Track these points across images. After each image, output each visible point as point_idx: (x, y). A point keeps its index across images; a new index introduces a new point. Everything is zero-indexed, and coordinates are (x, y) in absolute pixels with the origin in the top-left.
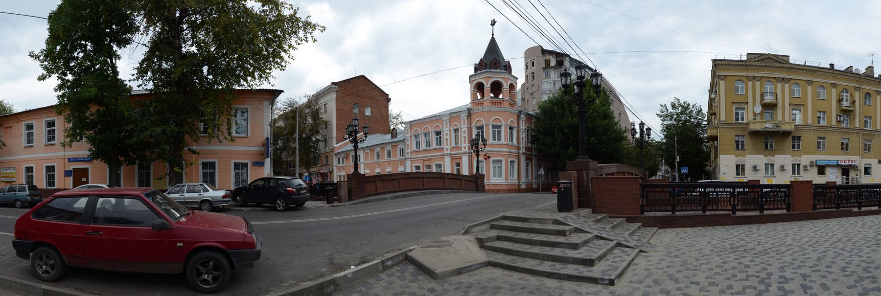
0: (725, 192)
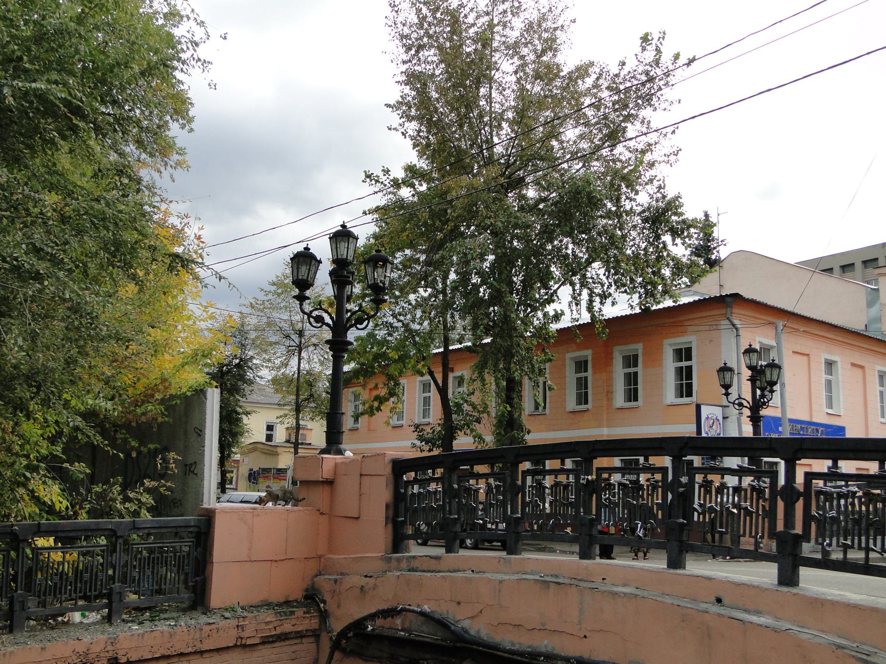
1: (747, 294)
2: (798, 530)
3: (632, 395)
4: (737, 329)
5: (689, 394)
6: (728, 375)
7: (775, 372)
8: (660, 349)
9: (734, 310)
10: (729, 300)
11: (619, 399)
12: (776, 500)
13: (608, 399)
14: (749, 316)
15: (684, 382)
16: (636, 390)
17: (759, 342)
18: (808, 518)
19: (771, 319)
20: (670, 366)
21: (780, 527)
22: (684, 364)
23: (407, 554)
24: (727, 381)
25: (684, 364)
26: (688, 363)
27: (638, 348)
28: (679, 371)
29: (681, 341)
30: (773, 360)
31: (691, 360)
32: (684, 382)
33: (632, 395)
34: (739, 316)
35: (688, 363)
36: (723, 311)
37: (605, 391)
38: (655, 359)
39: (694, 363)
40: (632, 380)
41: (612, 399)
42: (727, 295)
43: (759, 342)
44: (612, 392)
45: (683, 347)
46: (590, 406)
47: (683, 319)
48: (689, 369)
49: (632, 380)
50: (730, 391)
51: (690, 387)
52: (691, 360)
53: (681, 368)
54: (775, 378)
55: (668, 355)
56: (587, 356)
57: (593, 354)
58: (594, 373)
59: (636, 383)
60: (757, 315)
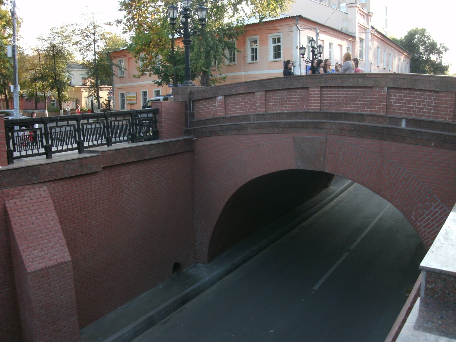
0: (88, 123)
1: (304, 16)
2: (12, 148)
3: (254, 58)
4: (299, 31)
5: (279, 57)
6: (303, 50)
7: (321, 49)
8: (267, 38)
9: (299, 22)
10: (297, 18)
11: (249, 59)
12: (12, 136)
13: (244, 60)
14: (303, 25)
15: (277, 52)
16: (256, 56)
17: (307, 35)
18: (14, 145)
19: (315, 27)
20: (271, 46)
21: (45, 144)
22: (277, 44)
23: (429, 104)
24: (303, 53)
25: (277, 44)
26: (279, 44)
27: (258, 37)
28: (253, 50)
29: (276, 35)
30: (320, 44)
31: (280, 43)
32: (277, 52)
33: (254, 58)
34: (300, 24)
35: (279, 44)
36: (295, 22)
37: (243, 56)
38: (264, 42)
39: (281, 44)
40: (254, 51)
41: (246, 60)
42: (296, 16)
43: (307, 35)
44: (246, 57)
45: (276, 37)
46: (236, 62)
47: (249, 29)
48: (279, 47)
49: (254, 51)
50: (304, 56)
51: (279, 54)
52: (280, 43)
53: (275, 46)
54: (321, 51)
55: (271, 41)
56: (257, 38)
57: (260, 38)
58: (260, 46)
59: (256, 52)
60: (307, 24)
